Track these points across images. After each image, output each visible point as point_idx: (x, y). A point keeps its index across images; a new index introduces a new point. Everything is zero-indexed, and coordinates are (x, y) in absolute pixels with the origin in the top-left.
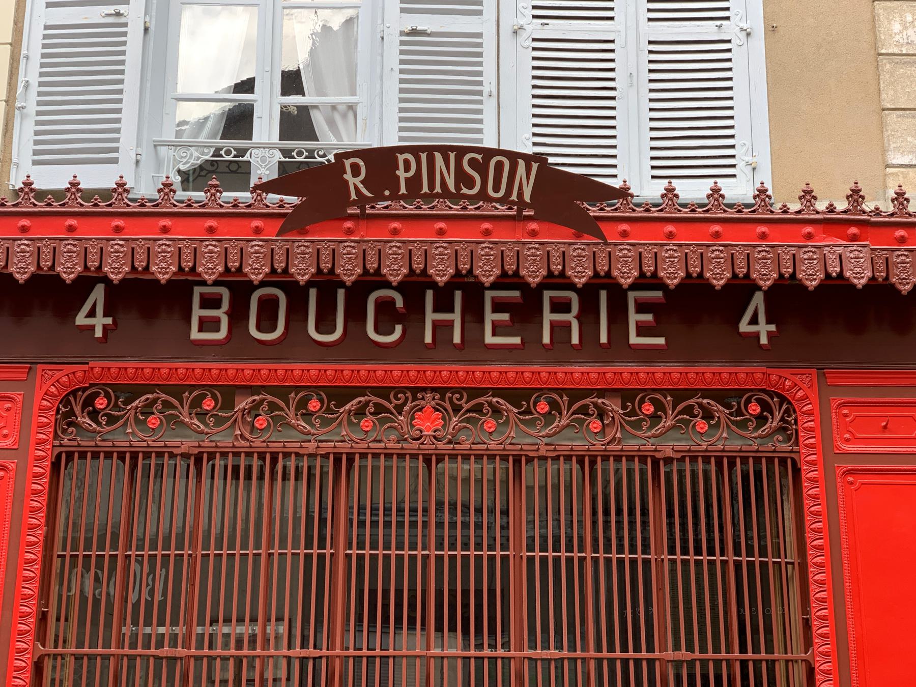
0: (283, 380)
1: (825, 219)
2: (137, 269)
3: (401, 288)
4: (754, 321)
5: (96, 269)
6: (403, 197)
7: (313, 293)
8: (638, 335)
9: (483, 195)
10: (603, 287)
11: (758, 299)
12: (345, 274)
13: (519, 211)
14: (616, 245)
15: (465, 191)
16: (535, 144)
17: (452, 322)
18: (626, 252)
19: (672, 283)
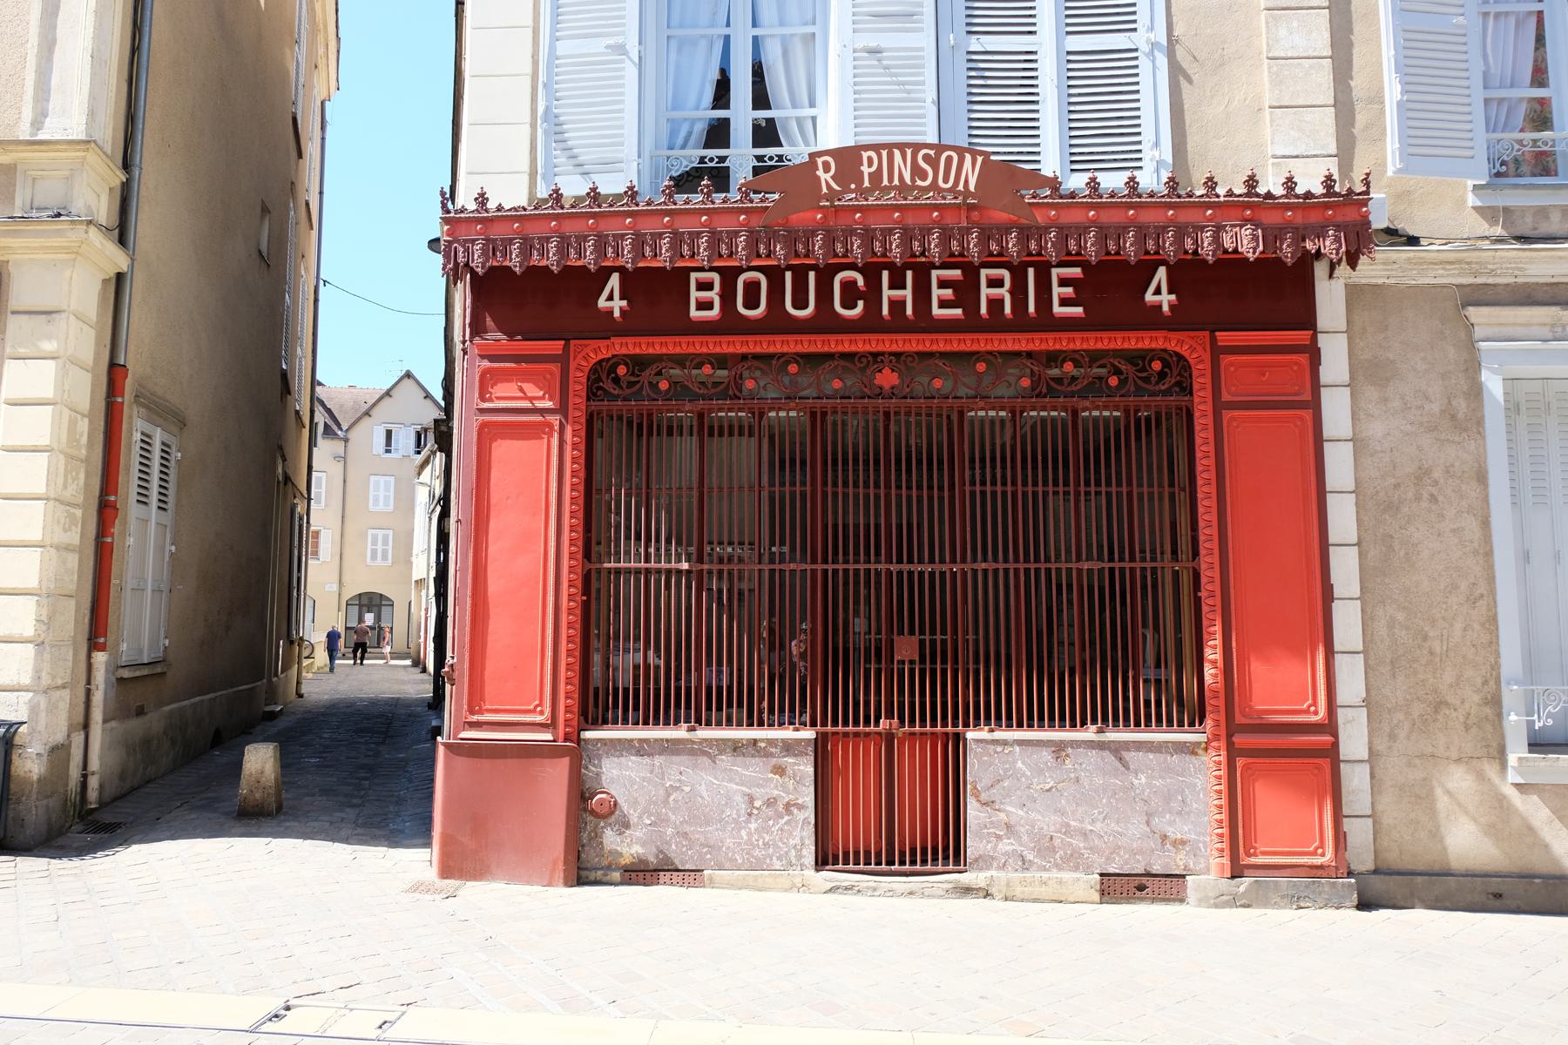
4: (1158, 291)
10: (1031, 264)
11: (1162, 273)
13: (965, 199)
15: (919, 183)
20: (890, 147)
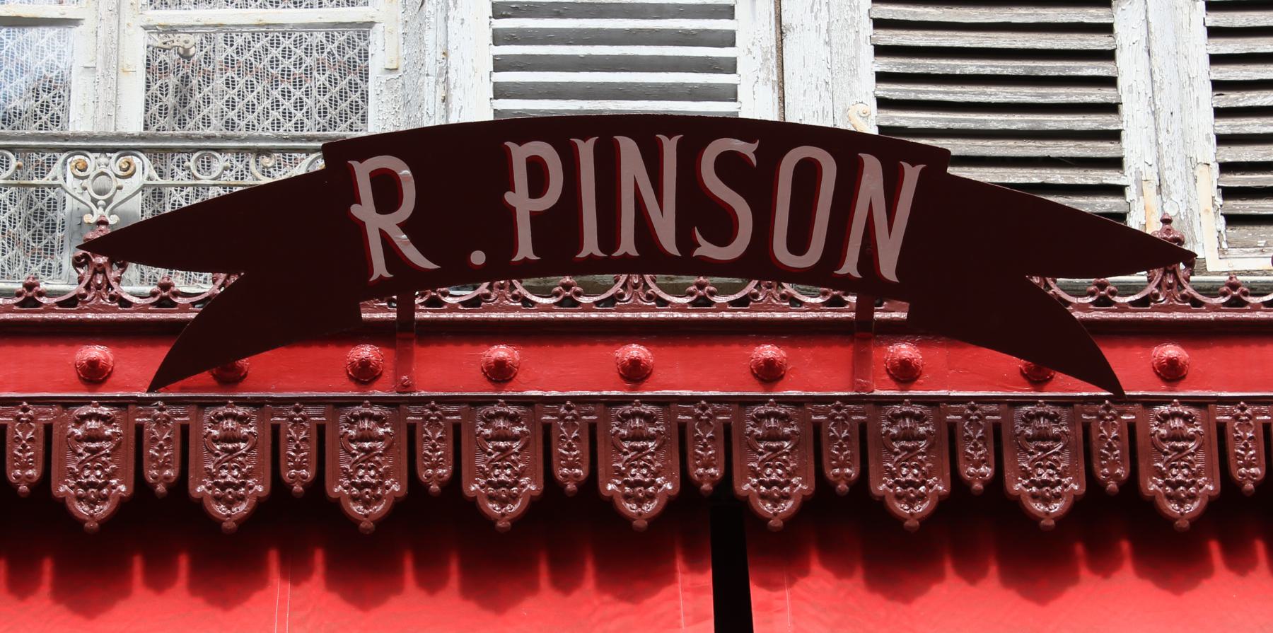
1: (1218, 322)
2: (425, 487)
6: (525, 270)
13: (864, 309)
15: (706, 249)
16: (883, 103)
18: (1043, 423)
20: (605, 129)
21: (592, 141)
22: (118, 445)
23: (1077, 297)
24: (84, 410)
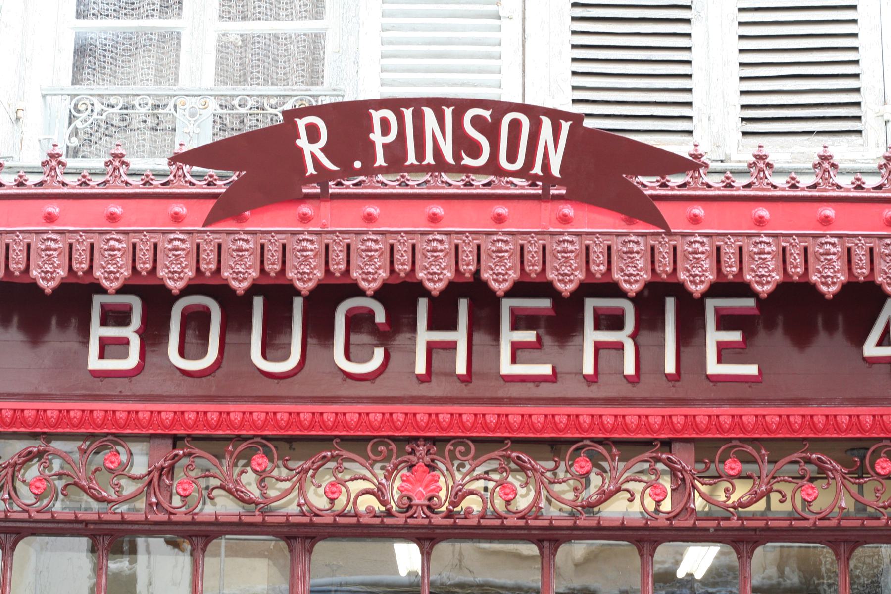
0: (216, 428)
2: (140, 273)
3: (378, 295)
5: (85, 273)
7: (258, 303)
8: (720, 361)
9: (493, 167)
12: (625, 281)
13: (545, 189)
14: (684, 235)
15: (467, 161)
17: (455, 343)
19: (764, 289)
20: (417, 104)
21: (411, 109)
22: (188, 252)
23: (649, 183)
24: (172, 236)
